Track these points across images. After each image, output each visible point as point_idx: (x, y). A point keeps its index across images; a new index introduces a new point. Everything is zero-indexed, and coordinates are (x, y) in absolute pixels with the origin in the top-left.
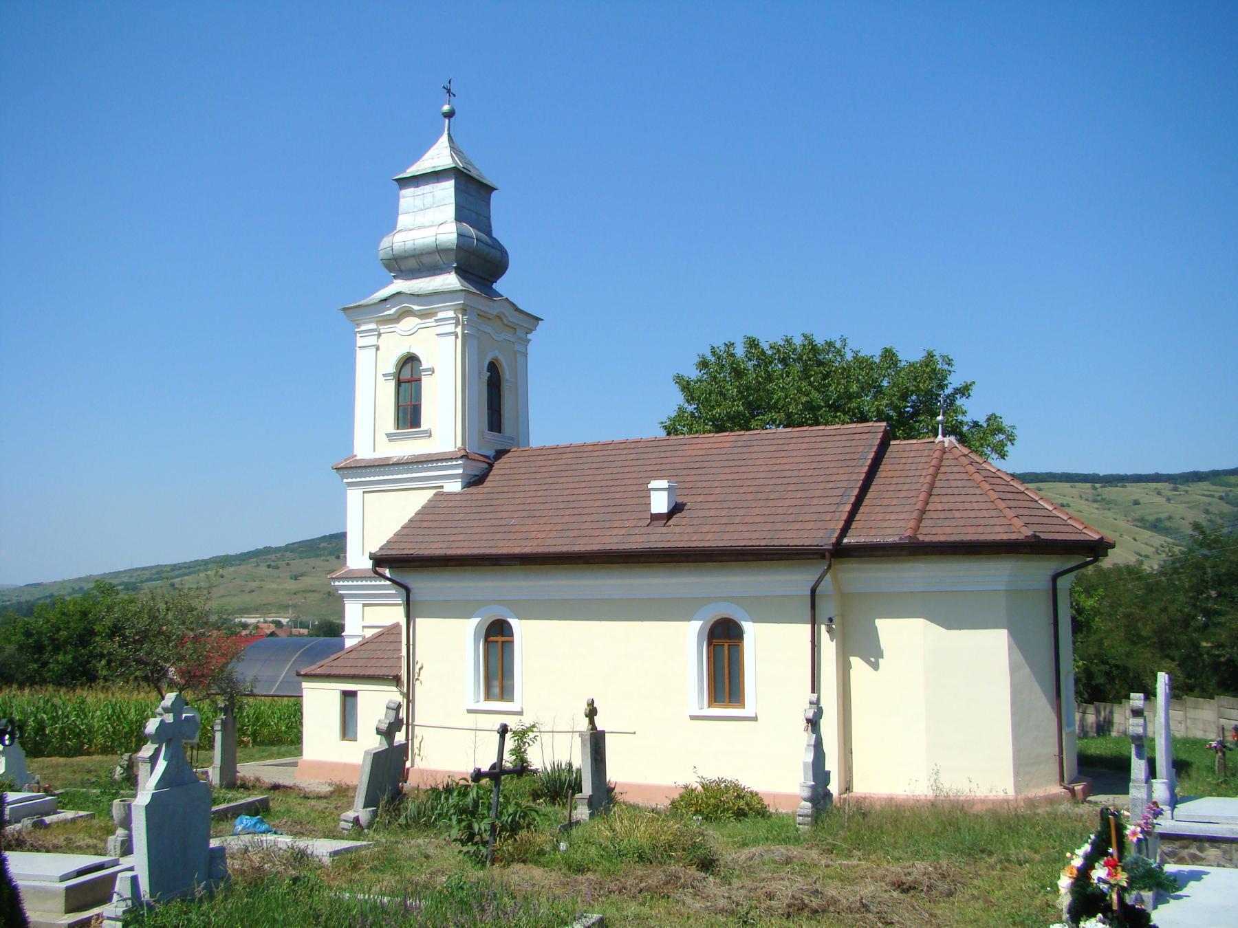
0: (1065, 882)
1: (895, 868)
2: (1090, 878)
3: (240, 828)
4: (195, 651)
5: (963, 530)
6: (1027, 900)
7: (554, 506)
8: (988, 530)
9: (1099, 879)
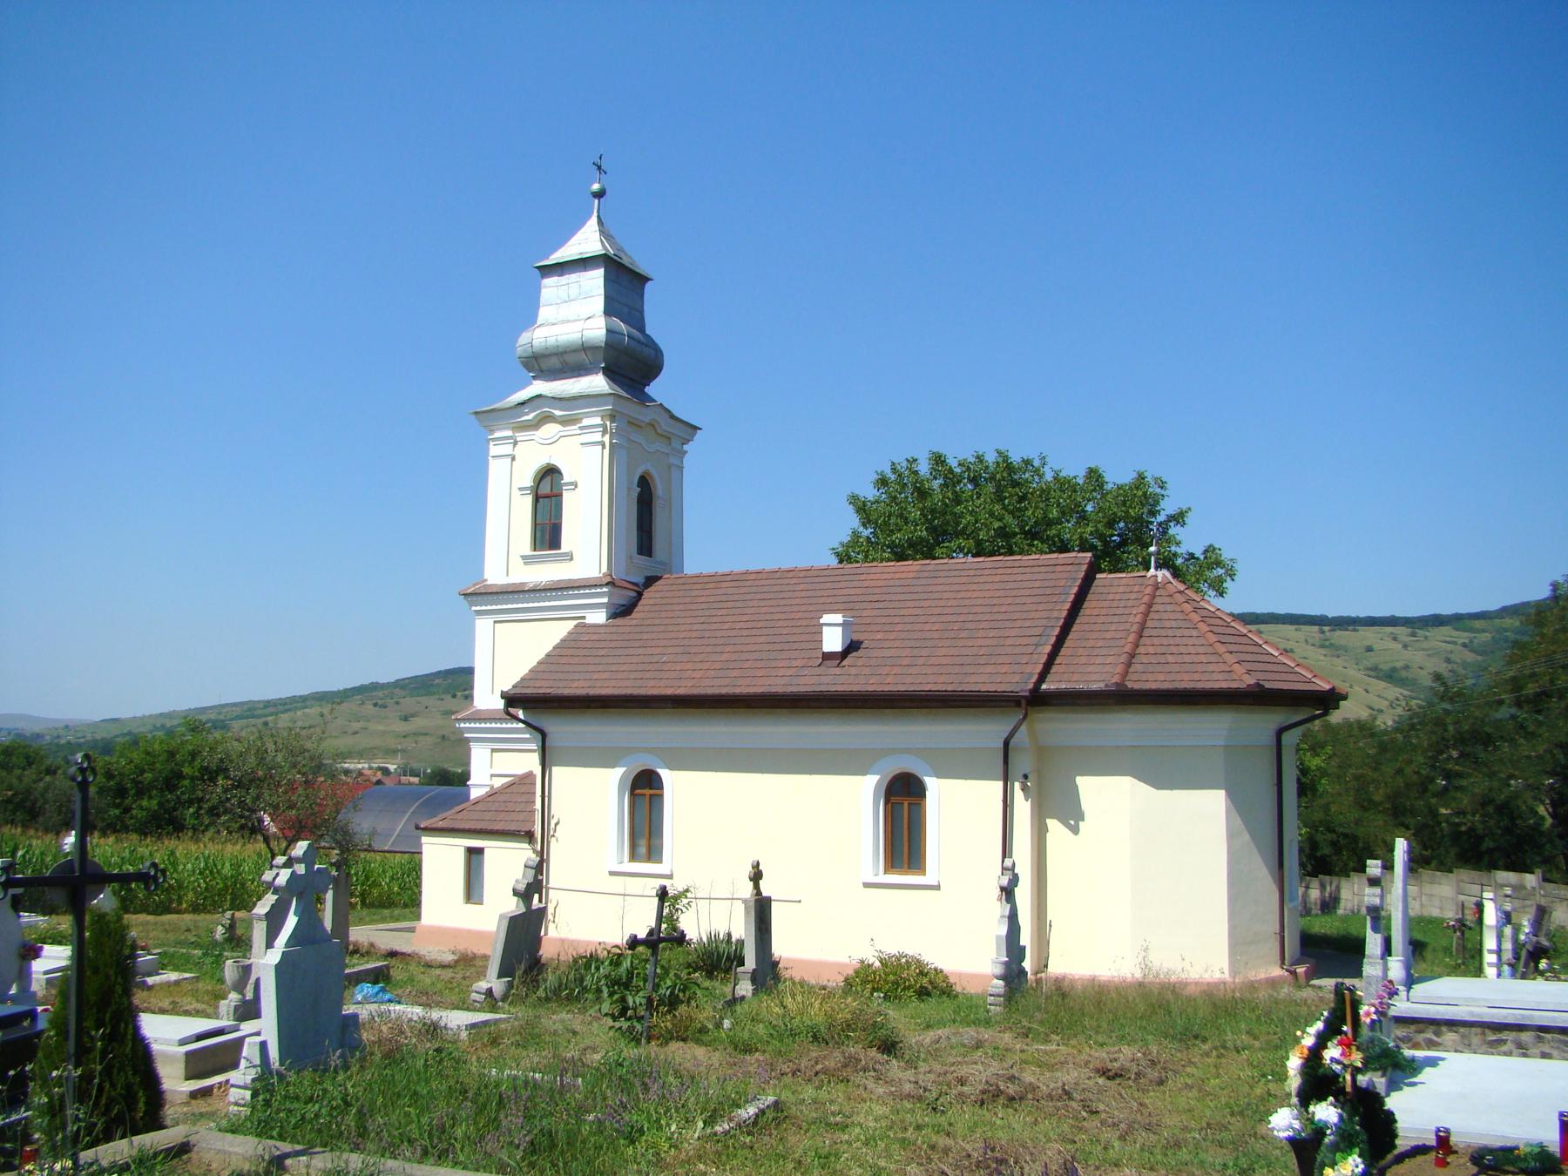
0: (1294, 1063)
1: (1102, 1054)
2: (1321, 1058)
3: (359, 997)
4: (307, 797)
5: (1178, 677)
6: (1246, 1089)
7: (712, 641)
8: (1207, 676)
9: (1332, 1059)
